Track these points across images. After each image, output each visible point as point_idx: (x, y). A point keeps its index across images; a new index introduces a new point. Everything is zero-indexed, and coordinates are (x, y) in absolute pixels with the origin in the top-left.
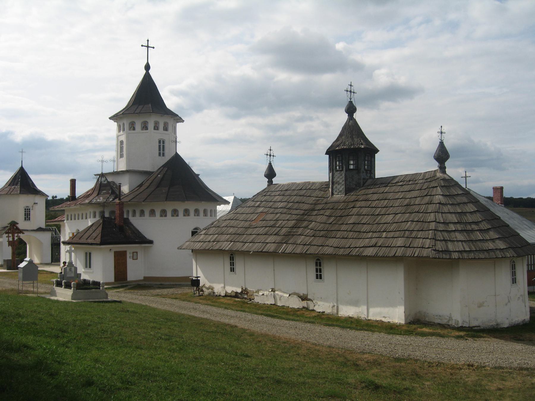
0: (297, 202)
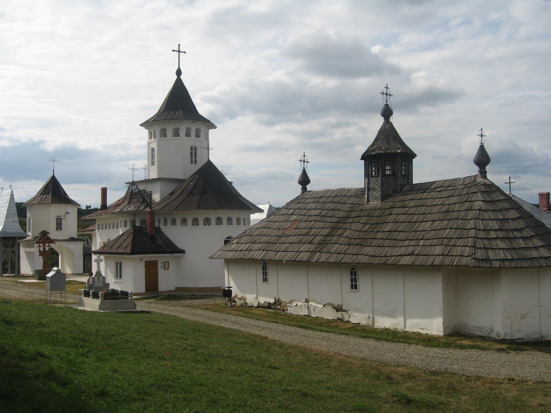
0: (332, 210)
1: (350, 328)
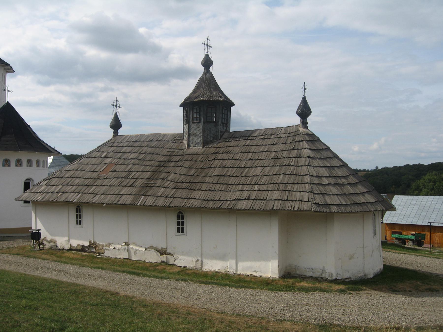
0: (150, 154)
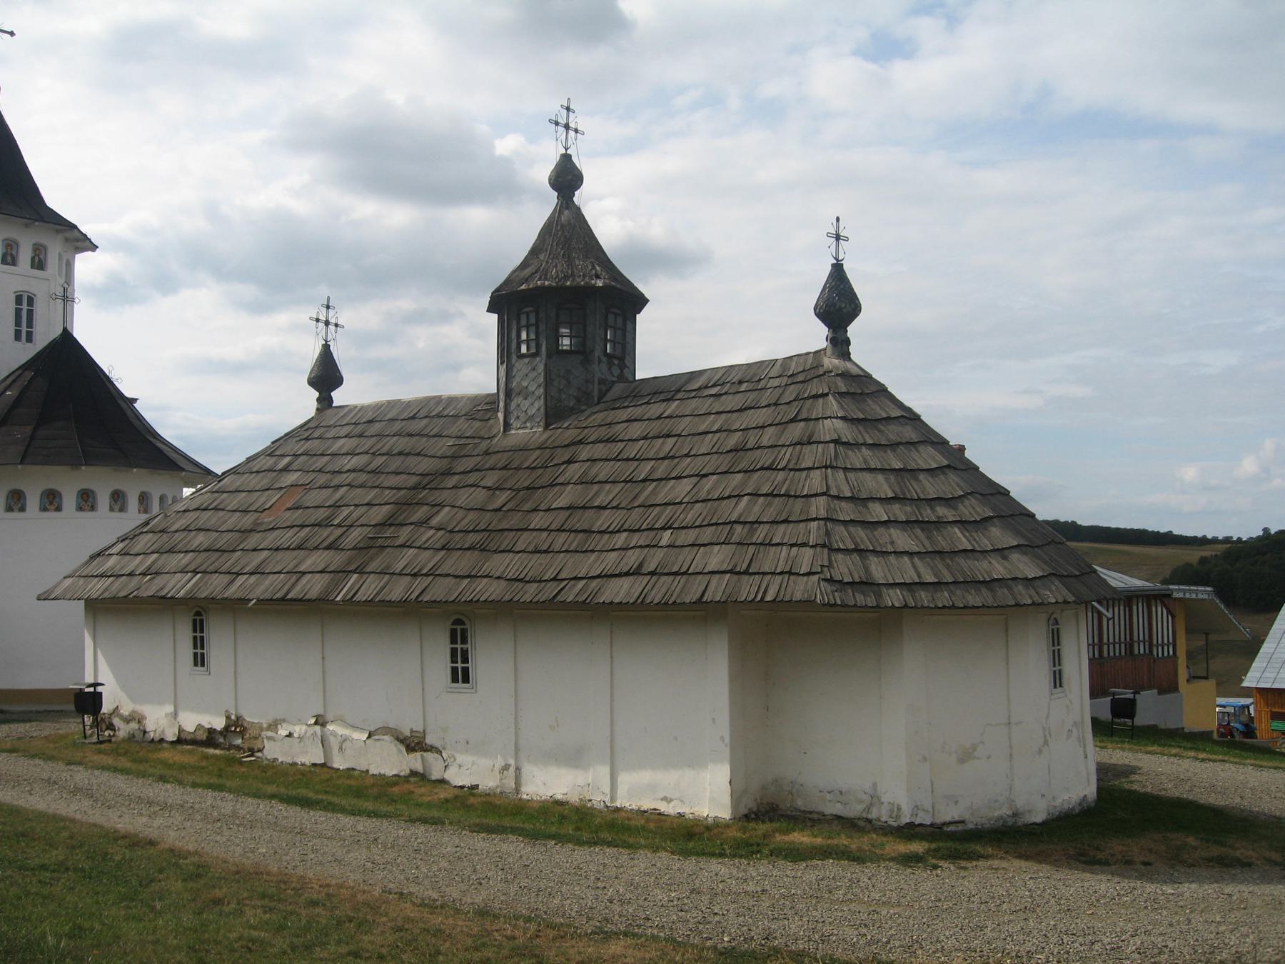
0: (400, 454)
1: (447, 801)
